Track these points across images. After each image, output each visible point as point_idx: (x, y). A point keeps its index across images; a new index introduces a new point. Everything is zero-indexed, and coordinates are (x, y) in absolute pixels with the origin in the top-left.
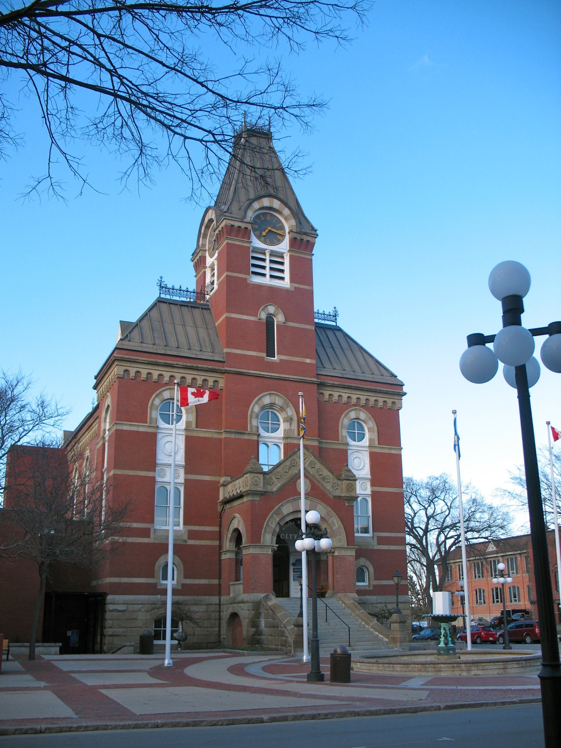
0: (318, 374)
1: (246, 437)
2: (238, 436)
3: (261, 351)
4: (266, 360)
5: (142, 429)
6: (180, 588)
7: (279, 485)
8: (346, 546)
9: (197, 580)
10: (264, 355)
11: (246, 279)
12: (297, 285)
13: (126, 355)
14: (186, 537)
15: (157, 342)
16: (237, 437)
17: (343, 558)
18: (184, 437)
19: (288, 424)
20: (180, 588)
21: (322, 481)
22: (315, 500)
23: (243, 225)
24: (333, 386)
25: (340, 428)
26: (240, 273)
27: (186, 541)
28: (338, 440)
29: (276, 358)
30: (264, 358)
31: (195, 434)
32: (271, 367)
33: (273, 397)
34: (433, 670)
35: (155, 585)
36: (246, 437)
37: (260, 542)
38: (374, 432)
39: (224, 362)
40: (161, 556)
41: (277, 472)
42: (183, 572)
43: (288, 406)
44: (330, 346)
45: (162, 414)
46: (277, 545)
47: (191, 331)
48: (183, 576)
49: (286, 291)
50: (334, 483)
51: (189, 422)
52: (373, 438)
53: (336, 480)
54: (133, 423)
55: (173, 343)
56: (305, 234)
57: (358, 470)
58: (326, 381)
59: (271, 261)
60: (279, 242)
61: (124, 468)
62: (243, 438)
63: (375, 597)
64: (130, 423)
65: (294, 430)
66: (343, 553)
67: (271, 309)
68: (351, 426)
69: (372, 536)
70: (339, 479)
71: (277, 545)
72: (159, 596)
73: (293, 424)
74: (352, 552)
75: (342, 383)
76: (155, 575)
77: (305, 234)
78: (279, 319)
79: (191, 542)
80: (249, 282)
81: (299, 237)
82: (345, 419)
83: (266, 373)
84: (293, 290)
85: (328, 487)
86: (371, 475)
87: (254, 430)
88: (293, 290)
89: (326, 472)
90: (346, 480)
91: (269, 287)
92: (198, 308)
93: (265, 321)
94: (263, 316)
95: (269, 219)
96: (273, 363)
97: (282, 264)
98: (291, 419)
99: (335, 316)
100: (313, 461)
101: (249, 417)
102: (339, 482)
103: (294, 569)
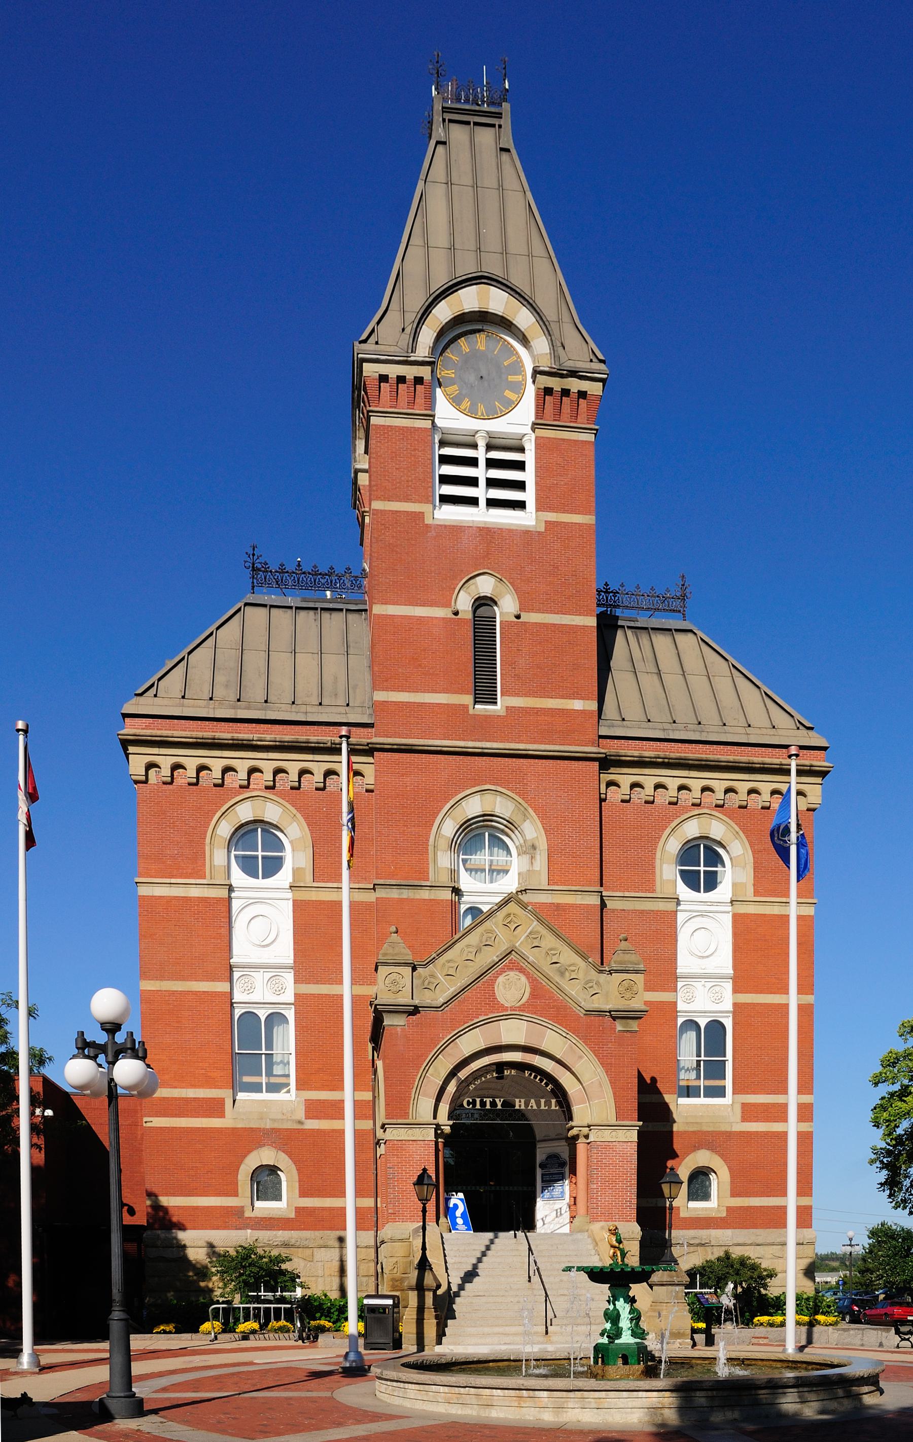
0: (601, 737)
1: (425, 894)
2: (406, 894)
3: (461, 691)
4: (471, 711)
5: (195, 892)
6: (293, 1215)
7: (452, 990)
8: (614, 1122)
9: (328, 1199)
10: (468, 699)
11: (420, 516)
12: (552, 516)
13: (147, 728)
14: (300, 1114)
15: (219, 693)
16: (405, 896)
17: (607, 1146)
18: (291, 902)
19: (526, 858)
20: (293, 1215)
21: (557, 978)
22: (537, 1018)
23: (410, 372)
24: (641, 763)
25: (658, 862)
26: (407, 499)
27: (300, 1122)
28: (654, 891)
29: (498, 708)
30: (466, 707)
31: (314, 896)
32: (485, 726)
33: (488, 797)
34: (474, 1400)
35: (239, 1211)
36: (425, 894)
37: (406, 1115)
38: (744, 867)
39: (371, 725)
40: (249, 1152)
41: (449, 961)
42: (297, 1185)
43: (525, 817)
44: (656, 671)
45: (244, 857)
46: (451, 1123)
47: (307, 663)
48: (297, 1191)
49: (526, 534)
50: (590, 981)
51: (298, 869)
52: (744, 880)
53: (593, 974)
54: (173, 881)
55: (256, 693)
56: (573, 374)
57: (707, 957)
58: (622, 752)
59: (492, 464)
60: (510, 406)
61: (162, 978)
62: (418, 897)
63: (729, 1232)
64: (168, 881)
65: (539, 872)
66: (607, 1135)
67: (485, 585)
68: (688, 853)
69: (730, 1102)
70: (601, 972)
71: (451, 1123)
72: (249, 1231)
73: (538, 857)
74: (629, 1133)
75: (662, 754)
76: (240, 1191)
77: (573, 374)
78: (507, 606)
79: (313, 1124)
80: (428, 521)
81: (556, 384)
82: (672, 838)
83: (470, 744)
84: (542, 528)
85: (574, 990)
86: (735, 967)
87: (444, 879)
88: (542, 528)
89: (568, 956)
90: (617, 971)
91: (480, 529)
92: (341, 610)
93: (470, 616)
94: (464, 603)
95: (483, 348)
96: (488, 719)
97: (520, 466)
98: (534, 847)
99: (683, 598)
100: (538, 932)
101: (431, 849)
102: (603, 977)
103: (543, 1175)
